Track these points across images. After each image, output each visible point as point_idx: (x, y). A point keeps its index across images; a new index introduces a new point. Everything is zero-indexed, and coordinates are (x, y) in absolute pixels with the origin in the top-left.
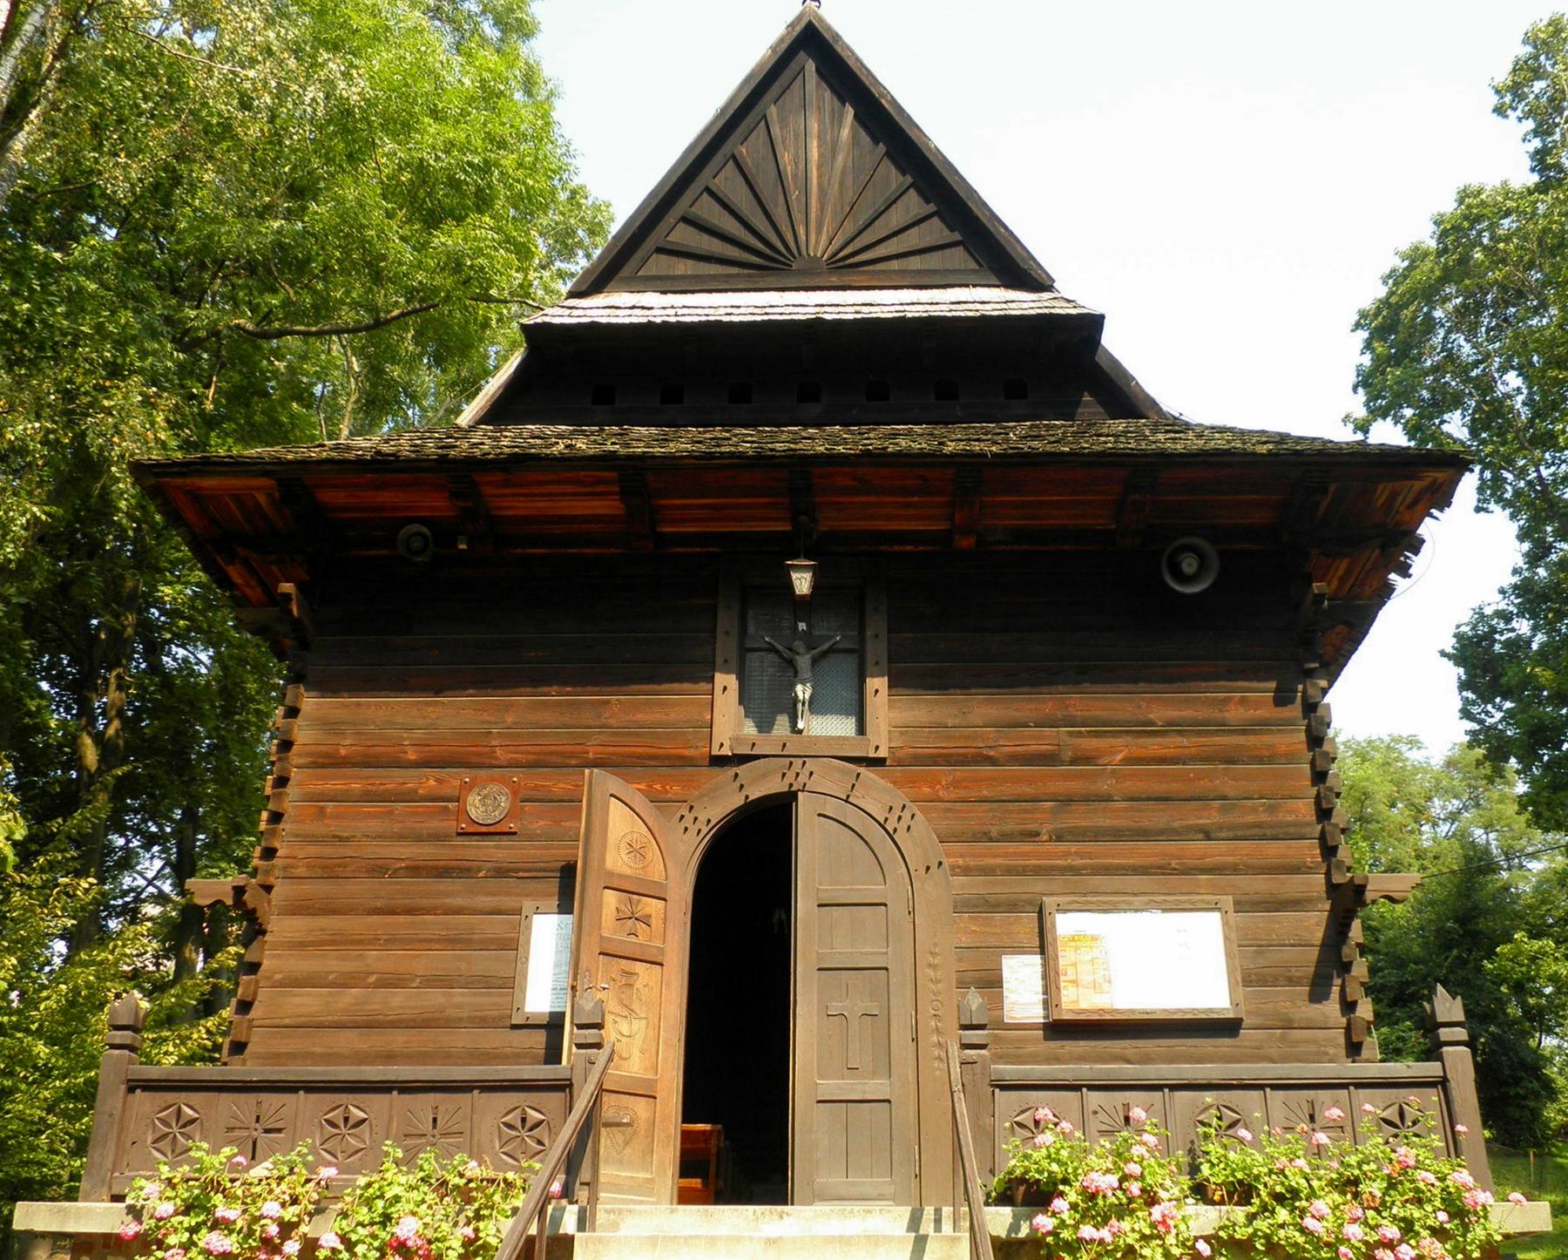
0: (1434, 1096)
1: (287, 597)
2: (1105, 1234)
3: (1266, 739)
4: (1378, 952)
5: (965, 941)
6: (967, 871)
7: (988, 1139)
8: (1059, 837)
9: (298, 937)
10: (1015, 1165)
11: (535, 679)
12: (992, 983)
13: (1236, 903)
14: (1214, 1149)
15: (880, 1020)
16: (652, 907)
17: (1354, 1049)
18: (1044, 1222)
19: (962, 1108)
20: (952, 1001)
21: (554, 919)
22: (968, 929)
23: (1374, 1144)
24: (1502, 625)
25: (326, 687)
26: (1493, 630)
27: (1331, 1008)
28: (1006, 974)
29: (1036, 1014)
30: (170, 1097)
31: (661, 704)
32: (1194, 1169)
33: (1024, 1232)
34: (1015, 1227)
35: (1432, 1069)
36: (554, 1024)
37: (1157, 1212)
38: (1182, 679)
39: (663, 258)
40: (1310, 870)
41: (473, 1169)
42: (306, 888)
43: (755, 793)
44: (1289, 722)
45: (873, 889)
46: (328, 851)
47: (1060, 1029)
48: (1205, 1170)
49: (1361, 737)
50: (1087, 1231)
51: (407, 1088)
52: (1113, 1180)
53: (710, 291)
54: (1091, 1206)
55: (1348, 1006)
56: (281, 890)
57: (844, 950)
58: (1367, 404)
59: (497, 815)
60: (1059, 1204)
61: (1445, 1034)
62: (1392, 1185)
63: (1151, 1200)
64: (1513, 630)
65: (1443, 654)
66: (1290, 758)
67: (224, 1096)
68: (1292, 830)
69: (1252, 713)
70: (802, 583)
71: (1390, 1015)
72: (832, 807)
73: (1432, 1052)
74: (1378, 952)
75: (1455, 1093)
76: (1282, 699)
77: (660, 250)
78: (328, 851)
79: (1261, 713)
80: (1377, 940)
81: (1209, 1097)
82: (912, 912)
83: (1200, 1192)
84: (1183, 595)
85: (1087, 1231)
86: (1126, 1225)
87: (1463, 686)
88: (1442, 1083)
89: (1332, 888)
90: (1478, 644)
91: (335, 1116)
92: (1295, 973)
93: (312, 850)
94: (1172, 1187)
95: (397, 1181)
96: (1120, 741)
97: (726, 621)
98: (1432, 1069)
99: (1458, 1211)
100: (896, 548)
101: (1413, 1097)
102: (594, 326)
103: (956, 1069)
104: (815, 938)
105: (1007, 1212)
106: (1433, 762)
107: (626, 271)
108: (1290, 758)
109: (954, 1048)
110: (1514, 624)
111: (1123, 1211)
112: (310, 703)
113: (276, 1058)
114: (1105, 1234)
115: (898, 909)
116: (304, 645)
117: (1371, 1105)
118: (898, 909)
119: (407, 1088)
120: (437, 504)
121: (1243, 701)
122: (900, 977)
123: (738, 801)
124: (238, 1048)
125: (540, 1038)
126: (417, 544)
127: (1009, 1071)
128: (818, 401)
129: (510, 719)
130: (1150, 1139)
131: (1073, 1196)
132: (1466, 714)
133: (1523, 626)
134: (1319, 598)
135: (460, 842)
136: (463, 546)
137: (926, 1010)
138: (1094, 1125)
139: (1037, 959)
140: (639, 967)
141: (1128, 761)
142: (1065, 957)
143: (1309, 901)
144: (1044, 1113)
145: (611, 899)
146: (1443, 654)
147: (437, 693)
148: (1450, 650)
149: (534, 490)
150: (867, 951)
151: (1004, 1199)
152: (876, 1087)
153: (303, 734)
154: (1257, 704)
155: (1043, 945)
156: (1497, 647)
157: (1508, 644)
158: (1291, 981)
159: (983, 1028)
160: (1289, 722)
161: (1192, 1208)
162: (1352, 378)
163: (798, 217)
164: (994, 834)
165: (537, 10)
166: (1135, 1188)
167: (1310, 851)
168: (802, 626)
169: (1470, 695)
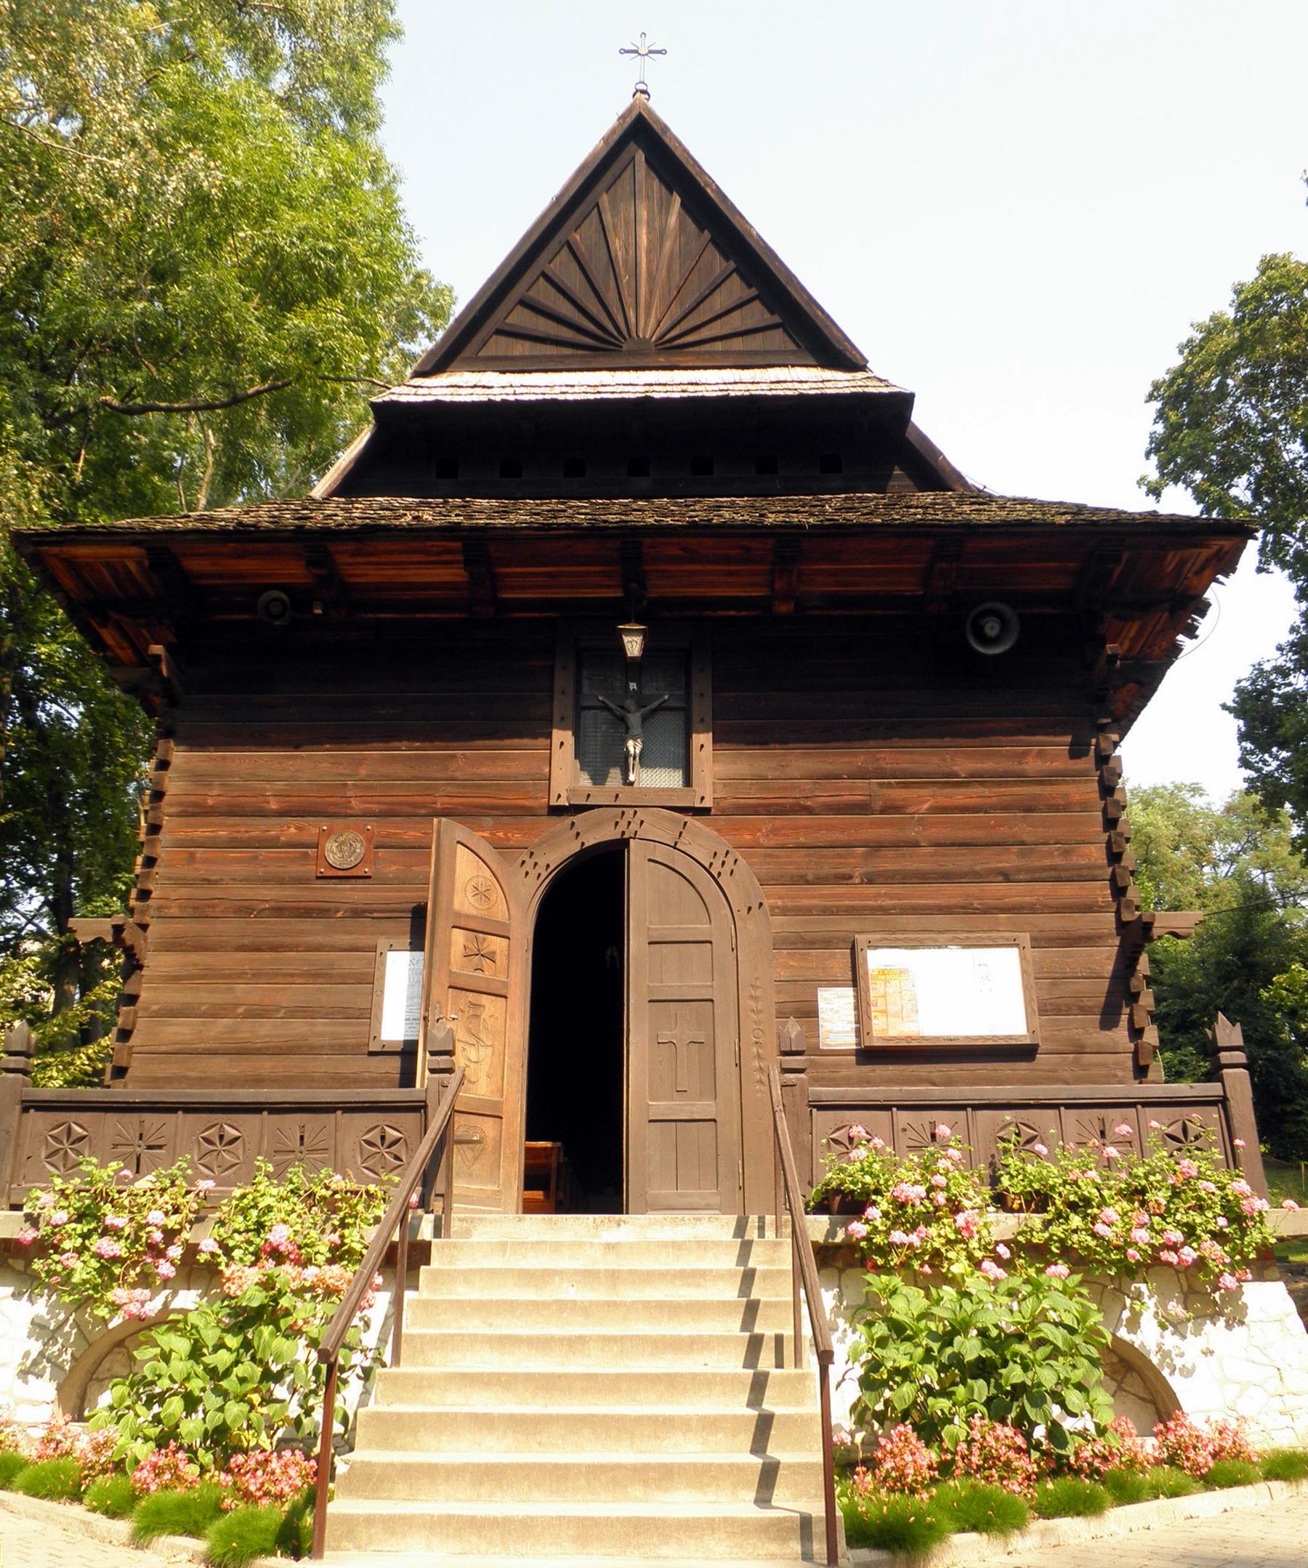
0: (1215, 1113)
1: (157, 658)
2: (914, 1239)
3: (1062, 789)
4: (1162, 984)
5: (784, 975)
6: (785, 911)
7: (806, 1154)
8: (870, 880)
10: (831, 1177)
11: (387, 733)
12: (809, 1013)
13: (1033, 939)
15: (706, 1047)
16: (497, 944)
17: (1141, 1072)
18: (859, 1228)
19: (783, 1125)
20: (767, 1033)
21: (407, 956)
22: (787, 965)
23: (1160, 1157)
24: (1280, 680)
25: (195, 741)
26: (1272, 684)
28: (821, 1005)
29: (848, 1041)
30: (61, 1116)
31: (507, 758)
32: (995, 1181)
34: (831, 1233)
35: (1213, 1089)
36: (408, 1052)
37: (961, 1219)
39: (503, 339)
41: (338, 1182)
43: (590, 840)
44: (1084, 774)
45: (701, 929)
47: (871, 1055)
48: (1005, 1181)
50: (898, 1236)
52: (921, 1190)
53: (546, 371)
54: (901, 1214)
55: (1136, 1033)
57: (673, 985)
59: (353, 860)
60: (872, 1212)
61: (1225, 1057)
63: (955, 1208)
65: (1224, 707)
66: (1084, 807)
67: (111, 1117)
68: (1085, 872)
70: (633, 646)
71: (1173, 1041)
72: (661, 853)
77: (499, 332)
81: (1008, 1116)
82: (735, 949)
83: (1000, 1201)
84: (986, 656)
85: (898, 1236)
86: (933, 1231)
87: (1243, 737)
89: (1122, 926)
91: (374, 1136)
93: (184, 892)
94: (974, 1196)
95: (269, 1193)
97: (562, 681)
100: (720, 613)
101: (1195, 1114)
103: (777, 1091)
104: (646, 972)
105: (825, 1218)
107: (468, 352)
108: (1084, 807)
111: (930, 1218)
112: (179, 756)
114: (914, 1239)
115: (722, 946)
116: (173, 702)
117: (1157, 1122)
118: (722, 946)
119: (329, 1108)
121: (1040, 755)
122: (724, 1008)
123: (575, 847)
124: (120, 1072)
125: (395, 1064)
128: (647, 474)
129: (363, 772)
131: (884, 1205)
132: (1245, 763)
134: (1112, 659)
135: (319, 884)
136: (318, 611)
138: (904, 1141)
139: (850, 992)
140: (485, 999)
142: (876, 991)
143: (1100, 937)
144: (858, 1131)
145: (459, 937)
146: (1224, 707)
147: (297, 747)
148: (1230, 703)
149: (394, 558)
150: (695, 985)
152: (703, 1108)
153: (173, 785)
155: (856, 979)
157: (1285, 697)
159: (801, 1054)
160: (1084, 774)
161: (993, 1215)
162: (1145, 444)
163: (629, 300)
164: (810, 877)
166: (941, 1198)
168: (633, 686)
169: (1249, 746)
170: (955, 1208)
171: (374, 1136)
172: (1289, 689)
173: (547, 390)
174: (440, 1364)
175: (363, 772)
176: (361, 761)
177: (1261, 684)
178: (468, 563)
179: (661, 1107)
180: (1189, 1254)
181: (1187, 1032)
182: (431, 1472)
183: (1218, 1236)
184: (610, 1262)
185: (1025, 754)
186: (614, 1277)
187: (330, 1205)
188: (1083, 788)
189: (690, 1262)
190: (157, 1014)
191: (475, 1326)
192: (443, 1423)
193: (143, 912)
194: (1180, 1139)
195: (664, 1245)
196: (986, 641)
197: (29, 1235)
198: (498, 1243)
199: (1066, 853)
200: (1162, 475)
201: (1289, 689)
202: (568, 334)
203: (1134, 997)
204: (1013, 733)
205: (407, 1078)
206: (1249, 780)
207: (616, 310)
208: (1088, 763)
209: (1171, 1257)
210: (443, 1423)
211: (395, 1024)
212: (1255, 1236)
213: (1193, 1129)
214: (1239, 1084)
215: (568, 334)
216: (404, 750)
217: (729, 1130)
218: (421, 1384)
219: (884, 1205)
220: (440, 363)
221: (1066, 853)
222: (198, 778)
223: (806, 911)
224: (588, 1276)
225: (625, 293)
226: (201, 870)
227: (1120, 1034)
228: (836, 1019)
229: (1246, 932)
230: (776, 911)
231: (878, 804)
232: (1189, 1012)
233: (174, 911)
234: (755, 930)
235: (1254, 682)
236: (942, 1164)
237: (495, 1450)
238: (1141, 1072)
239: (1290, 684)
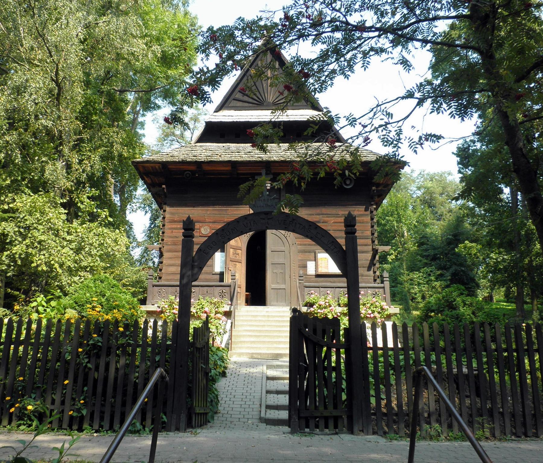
0: (381, 290)
1: (164, 188)
2: (322, 311)
3: (362, 218)
4: (428, 245)
5: (300, 258)
6: (301, 245)
7: (303, 296)
9: (170, 257)
10: (307, 300)
11: (214, 204)
12: (305, 267)
14: (342, 298)
15: (284, 274)
16: (239, 252)
17: (375, 280)
18: (312, 309)
19: (298, 290)
20: (296, 271)
21: (220, 253)
22: (301, 256)
23: (370, 298)
24: (472, 145)
25: (171, 205)
26: (469, 146)
27: (371, 272)
28: (308, 265)
29: (313, 273)
30: (160, 288)
31: (240, 210)
32: (339, 301)
33: (309, 311)
34: (307, 310)
35: (382, 285)
36: (222, 274)
37: (331, 308)
38: (346, 205)
39: (235, 101)
40: (369, 245)
41: (215, 300)
42: (171, 247)
44: (367, 215)
45: (282, 248)
46: (175, 239)
47: (318, 276)
48: (340, 301)
49: (431, 173)
50: (319, 311)
51: (202, 286)
52: (324, 303)
54: (320, 307)
55: (375, 272)
56: (166, 247)
57: (276, 260)
58: (432, 74)
59: (207, 233)
60: (314, 306)
61: (385, 279)
62: (372, 305)
63: (330, 306)
64: (475, 146)
65: (453, 153)
66: (367, 222)
67: (170, 288)
69: (360, 213)
71: (430, 264)
73: (382, 282)
74: (428, 245)
75: (386, 290)
76: (366, 210)
77: (234, 99)
78: (175, 239)
79: (362, 213)
80: (428, 241)
81: (342, 289)
82: (290, 253)
83: (339, 305)
85: (319, 311)
86: (326, 310)
87: (459, 163)
88: (384, 288)
89: (373, 249)
90: (464, 150)
91: (221, 292)
92: (365, 266)
93: (171, 239)
94: (333, 303)
95: (203, 302)
96: (332, 218)
98: (382, 285)
99: (382, 309)
101: (377, 290)
102: (221, 123)
103: (298, 284)
104: (271, 258)
105: (306, 308)
106: (456, 180)
107: (226, 105)
108: (367, 222)
109: (298, 281)
110: (476, 144)
111: (325, 308)
112: (168, 209)
113: (168, 280)
114: (322, 311)
115: (287, 252)
116: (166, 197)
117: (370, 291)
118: (287, 252)
119: (202, 286)
120: (193, 168)
121: (358, 210)
122: (287, 265)
124: (160, 278)
125: (218, 276)
126: (188, 175)
127: (307, 284)
129: (208, 213)
130: (330, 296)
131: (317, 305)
132: (460, 172)
133: (478, 145)
134: (374, 190)
135: (200, 238)
137: (292, 272)
138: (322, 294)
139: (314, 262)
140: (237, 263)
141: (334, 223)
142: (319, 262)
143: (368, 251)
144: (329, 292)
145: (232, 250)
146: (453, 153)
147: (194, 207)
148: (455, 152)
150: (281, 261)
151: (306, 306)
152: (283, 286)
153: (167, 216)
154: (361, 211)
155: (315, 259)
156: (471, 151)
157: (473, 150)
158: (364, 267)
159: (304, 276)
160: (367, 215)
161: (337, 307)
162: (428, 65)
163: (265, 91)
165: (190, 2)
166: (327, 304)
167: (370, 241)
169: (461, 166)
170: (330, 306)
171: (221, 292)
172: (475, 148)
173: (246, 117)
174: (240, 329)
175: (208, 213)
176: (208, 210)
177: (466, 146)
178: (232, 168)
179: (274, 286)
180: (372, 315)
181: (435, 261)
182: (244, 342)
183: (379, 313)
184: (267, 314)
185: (354, 210)
186: (268, 316)
187: (215, 304)
188: (367, 218)
189: (282, 314)
190: (167, 266)
191: (245, 323)
192: (244, 336)
193: (163, 244)
194: (375, 295)
195: (277, 311)
196: (347, 185)
197: (159, 310)
198: (245, 312)
199: (362, 233)
200: (433, 77)
201: (475, 148)
202: (251, 100)
203: (375, 265)
204: (351, 205)
205: (222, 280)
206: (462, 178)
207: (262, 94)
208: (369, 212)
209: (369, 316)
210: (244, 336)
211: (218, 269)
212: (386, 313)
213: (378, 293)
214: (387, 284)
215: (251, 100)
216: (217, 208)
217: (288, 291)
218: (239, 331)
219: (317, 305)
220: (220, 108)
221: (362, 233)
222: (172, 214)
223: (305, 245)
224: (264, 316)
225: (265, 89)
226: (174, 234)
227: (371, 272)
228: (311, 268)
229: (457, 229)
230: (298, 245)
231: (322, 221)
232: (437, 254)
233: (169, 243)
234: (294, 249)
235: (463, 145)
236: (328, 298)
237: (252, 339)
238: (375, 280)
239: (475, 146)
